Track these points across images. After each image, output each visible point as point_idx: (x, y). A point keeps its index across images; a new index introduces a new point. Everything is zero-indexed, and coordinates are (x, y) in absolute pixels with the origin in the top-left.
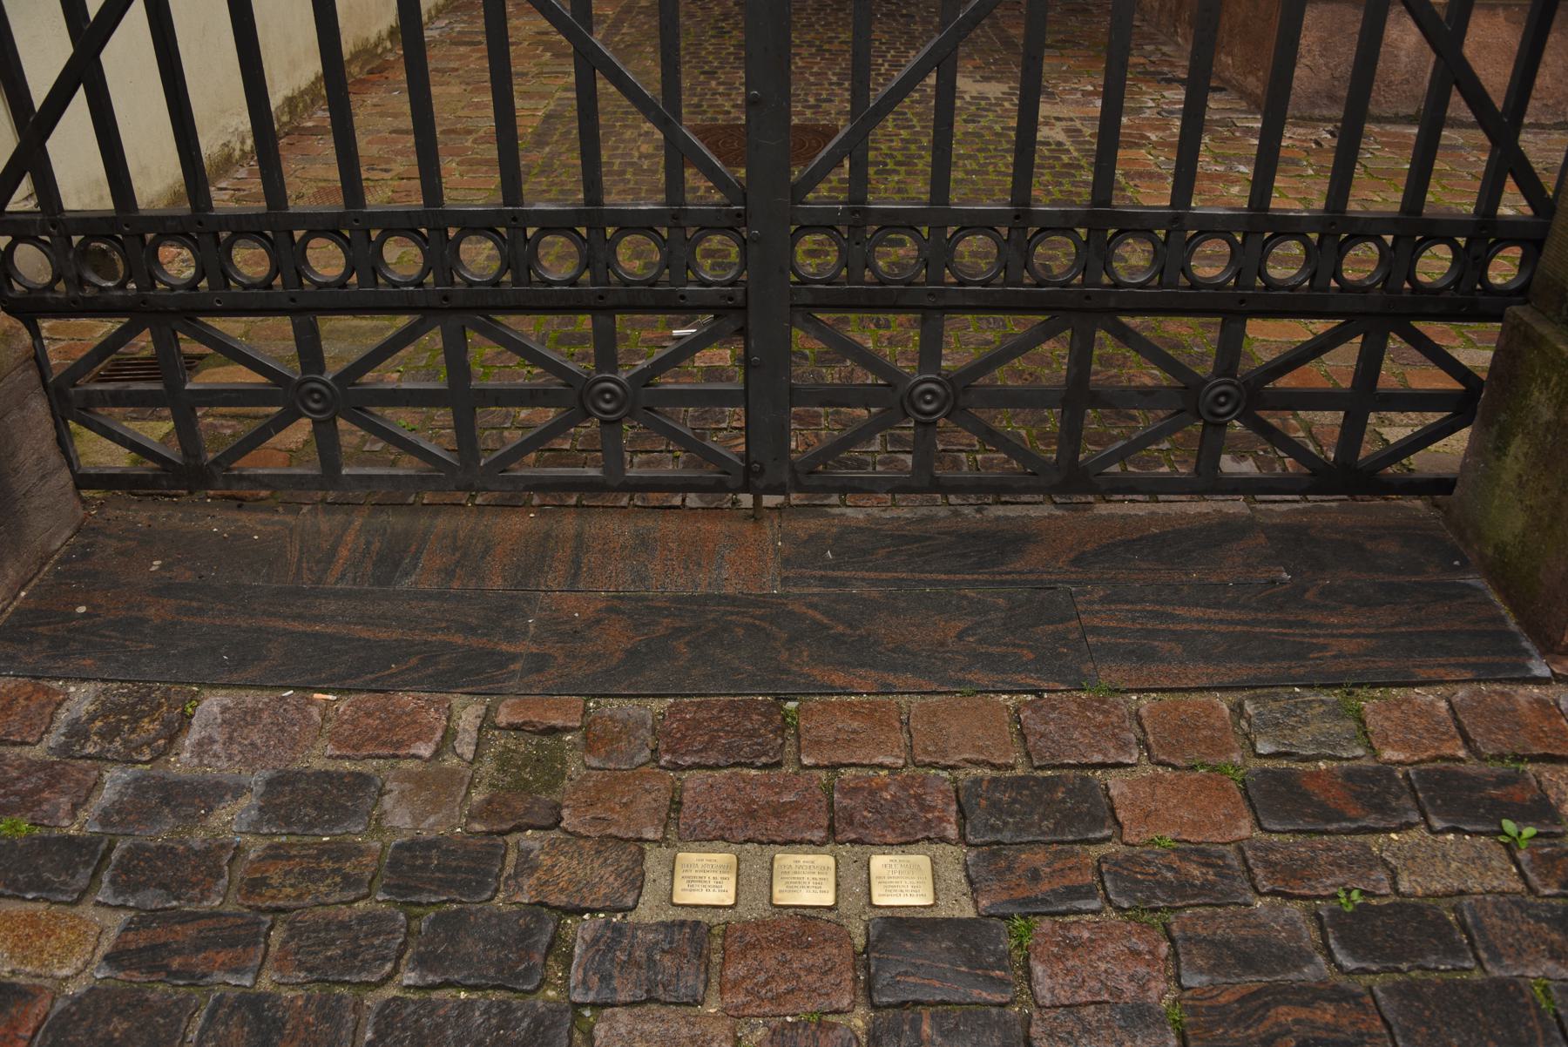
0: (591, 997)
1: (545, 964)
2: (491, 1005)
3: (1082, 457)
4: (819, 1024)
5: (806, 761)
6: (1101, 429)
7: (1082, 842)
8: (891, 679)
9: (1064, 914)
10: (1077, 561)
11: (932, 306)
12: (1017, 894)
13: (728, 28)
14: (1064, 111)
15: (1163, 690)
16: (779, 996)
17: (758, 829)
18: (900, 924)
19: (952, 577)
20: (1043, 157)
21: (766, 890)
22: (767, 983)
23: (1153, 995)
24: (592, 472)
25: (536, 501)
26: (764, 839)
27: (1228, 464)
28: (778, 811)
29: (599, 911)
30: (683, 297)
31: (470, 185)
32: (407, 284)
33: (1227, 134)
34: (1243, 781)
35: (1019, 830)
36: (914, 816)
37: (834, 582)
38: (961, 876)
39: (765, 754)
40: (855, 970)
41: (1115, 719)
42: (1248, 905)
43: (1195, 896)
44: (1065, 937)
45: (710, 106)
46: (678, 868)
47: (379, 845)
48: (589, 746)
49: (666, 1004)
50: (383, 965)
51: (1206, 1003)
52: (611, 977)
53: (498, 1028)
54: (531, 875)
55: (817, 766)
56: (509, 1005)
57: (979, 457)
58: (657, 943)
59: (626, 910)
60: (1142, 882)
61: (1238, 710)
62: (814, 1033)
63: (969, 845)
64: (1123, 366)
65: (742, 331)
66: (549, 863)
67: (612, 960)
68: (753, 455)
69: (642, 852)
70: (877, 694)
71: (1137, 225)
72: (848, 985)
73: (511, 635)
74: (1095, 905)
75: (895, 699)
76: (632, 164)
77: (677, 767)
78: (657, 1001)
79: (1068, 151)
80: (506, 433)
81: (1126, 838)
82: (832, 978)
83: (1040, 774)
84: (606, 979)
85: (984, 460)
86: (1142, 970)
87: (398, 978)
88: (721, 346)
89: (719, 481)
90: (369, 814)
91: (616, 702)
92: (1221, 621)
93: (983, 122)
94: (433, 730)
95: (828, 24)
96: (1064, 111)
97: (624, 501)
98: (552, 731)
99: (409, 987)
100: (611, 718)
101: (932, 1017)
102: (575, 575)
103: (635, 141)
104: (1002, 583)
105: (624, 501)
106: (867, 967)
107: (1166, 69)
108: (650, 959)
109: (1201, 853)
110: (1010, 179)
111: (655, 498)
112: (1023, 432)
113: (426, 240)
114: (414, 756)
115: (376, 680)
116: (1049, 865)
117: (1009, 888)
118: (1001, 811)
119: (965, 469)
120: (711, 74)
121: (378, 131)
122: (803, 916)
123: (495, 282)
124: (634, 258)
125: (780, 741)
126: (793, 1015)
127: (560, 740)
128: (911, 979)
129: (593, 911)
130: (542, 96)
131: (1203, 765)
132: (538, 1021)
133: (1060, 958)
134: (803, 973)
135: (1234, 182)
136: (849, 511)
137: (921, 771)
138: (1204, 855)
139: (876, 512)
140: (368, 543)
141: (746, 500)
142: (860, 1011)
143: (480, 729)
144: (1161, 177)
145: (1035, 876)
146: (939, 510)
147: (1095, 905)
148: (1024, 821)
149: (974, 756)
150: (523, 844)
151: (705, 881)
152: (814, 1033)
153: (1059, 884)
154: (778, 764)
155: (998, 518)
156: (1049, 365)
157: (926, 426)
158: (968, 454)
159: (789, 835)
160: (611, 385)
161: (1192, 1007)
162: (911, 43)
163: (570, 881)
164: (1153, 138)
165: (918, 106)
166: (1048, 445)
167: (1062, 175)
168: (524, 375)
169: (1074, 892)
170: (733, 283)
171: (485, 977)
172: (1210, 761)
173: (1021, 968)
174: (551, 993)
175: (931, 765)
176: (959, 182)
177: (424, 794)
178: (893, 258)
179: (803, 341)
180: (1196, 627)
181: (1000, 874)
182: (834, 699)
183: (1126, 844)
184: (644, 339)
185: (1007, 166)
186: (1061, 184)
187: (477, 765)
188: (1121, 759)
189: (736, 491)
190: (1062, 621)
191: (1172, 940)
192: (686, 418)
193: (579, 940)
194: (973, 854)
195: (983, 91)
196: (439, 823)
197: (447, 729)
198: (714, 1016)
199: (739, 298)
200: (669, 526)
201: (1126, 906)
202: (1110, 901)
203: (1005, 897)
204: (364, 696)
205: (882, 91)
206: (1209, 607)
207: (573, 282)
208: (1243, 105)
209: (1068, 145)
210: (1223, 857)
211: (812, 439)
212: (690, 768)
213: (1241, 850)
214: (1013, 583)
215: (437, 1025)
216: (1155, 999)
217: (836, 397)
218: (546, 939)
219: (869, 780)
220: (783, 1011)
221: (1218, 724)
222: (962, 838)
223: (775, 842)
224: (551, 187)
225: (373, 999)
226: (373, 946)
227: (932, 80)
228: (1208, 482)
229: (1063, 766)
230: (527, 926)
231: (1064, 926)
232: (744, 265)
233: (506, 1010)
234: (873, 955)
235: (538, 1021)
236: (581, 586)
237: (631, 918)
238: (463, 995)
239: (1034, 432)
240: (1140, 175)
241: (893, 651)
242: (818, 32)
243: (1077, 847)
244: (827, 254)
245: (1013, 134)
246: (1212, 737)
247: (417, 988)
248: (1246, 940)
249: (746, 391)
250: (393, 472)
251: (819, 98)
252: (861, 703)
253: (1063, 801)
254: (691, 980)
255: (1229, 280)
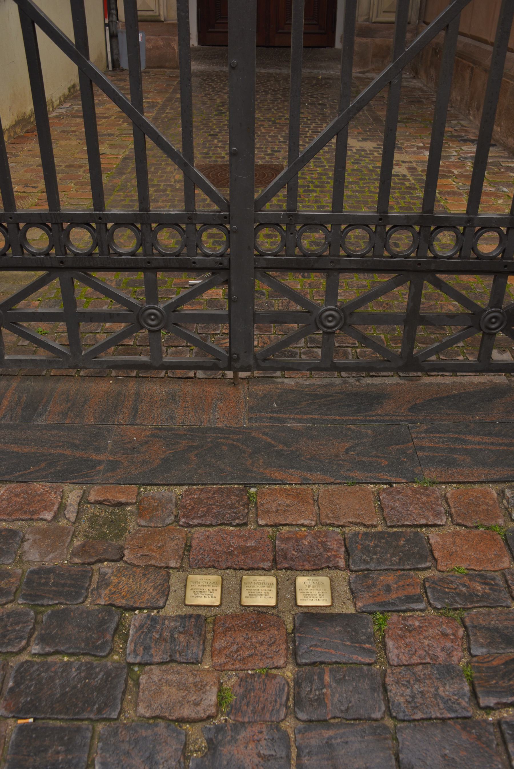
0: (138, 660)
1: (113, 640)
2: (81, 665)
3: (415, 351)
4: (267, 675)
5: (261, 522)
6: (426, 335)
7: (414, 569)
8: (308, 475)
9: (404, 611)
10: (411, 409)
11: (333, 268)
12: (378, 600)
13: (224, 111)
14: (407, 157)
15: (460, 483)
16: (244, 659)
17: (233, 564)
18: (313, 617)
19: (343, 418)
20: (395, 183)
21: (237, 597)
22: (237, 651)
23: (455, 659)
24: (144, 358)
25: (114, 374)
26: (237, 567)
27: (496, 355)
28: (245, 550)
29: (144, 609)
30: (194, 263)
31: (75, 198)
32: (40, 254)
33: (497, 170)
34: (505, 535)
35: (379, 563)
36: (321, 554)
37: (278, 420)
38: (347, 588)
39: (238, 518)
40: (287, 643)
41: (433, 499)
42: (508, 607)
43: (478, 602)
44: (405, 625)
45: (214, 154)
46: (189, 584)
47: (20, 571)
48: (140, 515)
49: (181, 663)
50: (20, 642)
51: (485, 665)
52: (150, 647)
53: (85, 678)
54: (106, 588)
55: (267, 525)
56: (92, 664)
57: (358, 350)
58: (176, 628)
59: (159, 608)
60: (448, 593)
61: (502, 494)
62: (264, 681)
63: (351, 571)
64: (437, 300)
65: (227, 282)
66: (116, 581)
67: (151, 638)
68: (233, 350)
69: (169, 575)
70: (301, 484)
71: (446, 223)
72: (283, 652)
73: (98, 450)
74: (422, 606)
75: (310, 487)
76: (171, 186)
77: (189, 526)
78: (176, 661)
79: (409, 180)
80: (98, 336)
81: (439, 568)
82: (274, 648)
83: (391, 530)
84: (147, 648)
85: (361, 352)
86: (449, 644)
87: (29, 649)
88: (217, 288)
89: (214, 364)
90: (15, 553)
91: (155, 488)
92: (492, 444)
93: (363, 164)
94: (53, 504)
95: (279, 109)
96: (407, 157)
97: (162, 374)
98: (120, 505)
99: (35, 654)
100: (153, 497)
101: (331, 671)
102: (135, 415)
103: (172, 173)
104: (371, 421)
105: (162, 374)
106: (294, 641)
107: (463, 134)
108: (172, 637)
109: (481, 576)
110: (377, 195)
111: (179, 373)
112: (383, 337)
113: (50, 229)
114: (42, 519)
115: (22, 476)
116: (396, 583)
117: (374, 596)
118: (369, 552)
119: (350, 357)
120: (215, 136)
121: (31, 165)
122: (258, 611)
123: (90, 254)
124: (168, 240)
125: (246, 511)
126: (252, 670)
127: (124, 510)
128: (319, 649)
129: (140, 609)
130: (122, 147)
131: (482, 526)
132: (108, 674)
133: (402, 637)
134: (258, 645)
135: (500, 197)
136: (286, 381)
137: (325, 528)
138: (484, 579)
139: (301, 381)
140: (20, 398)
141: (230, 374)
142: (290, 667)
143: (79, 504)
144: (460, 194)
145: (388, 589)
146: (336, 380)
147: (422, 606)
148: (382, 556)
149: (355, 520)
150: (102, 570)
151: (204, 591)
152: (264, 681)
153: (401, 594)
154: (246, 524)
155: (368, 385)
156: (397, 299)
157: (329, 334)
158: (352, 350)
159: (250, 565)
160: (155, 311)
161: (478, 667)
162: (324, 119)
163: (128, 592)
164: (456, 172)
165: (327, 155)
166: (396, 344)
167: (405, 193)
168: (107, 305)
169: (410, 599)
170: (222, 255)
171: (78, 648)
172: (486, 523)
173: (380, 642)
174: (116, 657)
175: (330, 525)
176: (349, 197)
177: (47, 542)
178: (312, 239)
179: (260, 285)
180: (478, 447)
181: (369, 587)
182: (277, 487)
183: (439, 571)
184: (174, 285)
185: (375, 188)
186: (405, 198)
187: (77, 524)
188: (436, 522)
189: (224, 369)
190: (403, 443)
191: (466, 627)
192: (196, 330)
193: (132, 626)
194: (353, 576)
195: (363, 147)
196: (55, 558)
197: (61, 504)
198: (208, 671)
199: (226, 263)
200: (187, 388)
201: (439, 607)
202: (430, 604)
203: (371, 601)
204: (15, 485)
205: (308, 147)
206: (485, 435)
207: (133, 254)
208: (506, 154)
209: (409, 176)
210: (494, 579)
211: (266, 340)
212: (196, 526)
213: (504, 575)
214: (377, 421)
215: (50, 677)
216: (456, 662)
217: (279, 318)
218: (113, 626)
219: (296, 533)
220: (246, 667)
221: (491, 503)
222: (348, 566)
223: (243, 569)
224: (120, 202)
225: (14, 662)
226: (15, 631)
227: (334, 140)
228: (485, 365)
229: (404, 526)
230: (103, 618)
231: (405, 619)
232: (229, 244)
233: (90, 667)
234: (297, 635)
235: (108, 674)
236: (138, 422)
237: (162, 613)
238: (66, 659)
239: (389, 336)
240: (448, 193)
241: (310, 459)
242: (273, 113)
243: (412, 573)
244: (276, 236)
245: (379, 170)
246: (487, 510)
247: (40, 655)
248: (508, 628)
249: (229, 315)
250: (34, 358)
251: (270, 149)
252: (292, 489)
253: (404, 546)
254: (195, 649)
255: (498, 254)
